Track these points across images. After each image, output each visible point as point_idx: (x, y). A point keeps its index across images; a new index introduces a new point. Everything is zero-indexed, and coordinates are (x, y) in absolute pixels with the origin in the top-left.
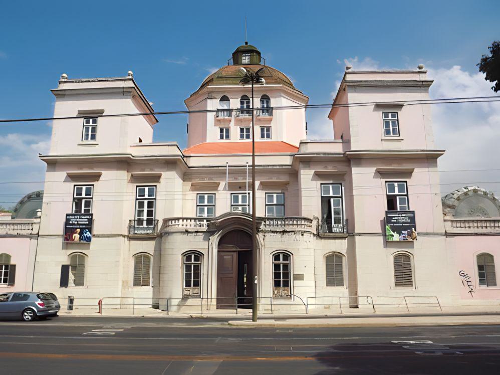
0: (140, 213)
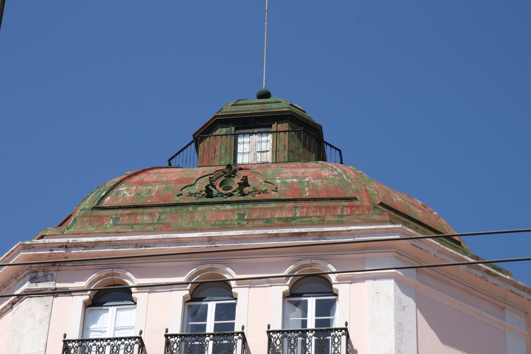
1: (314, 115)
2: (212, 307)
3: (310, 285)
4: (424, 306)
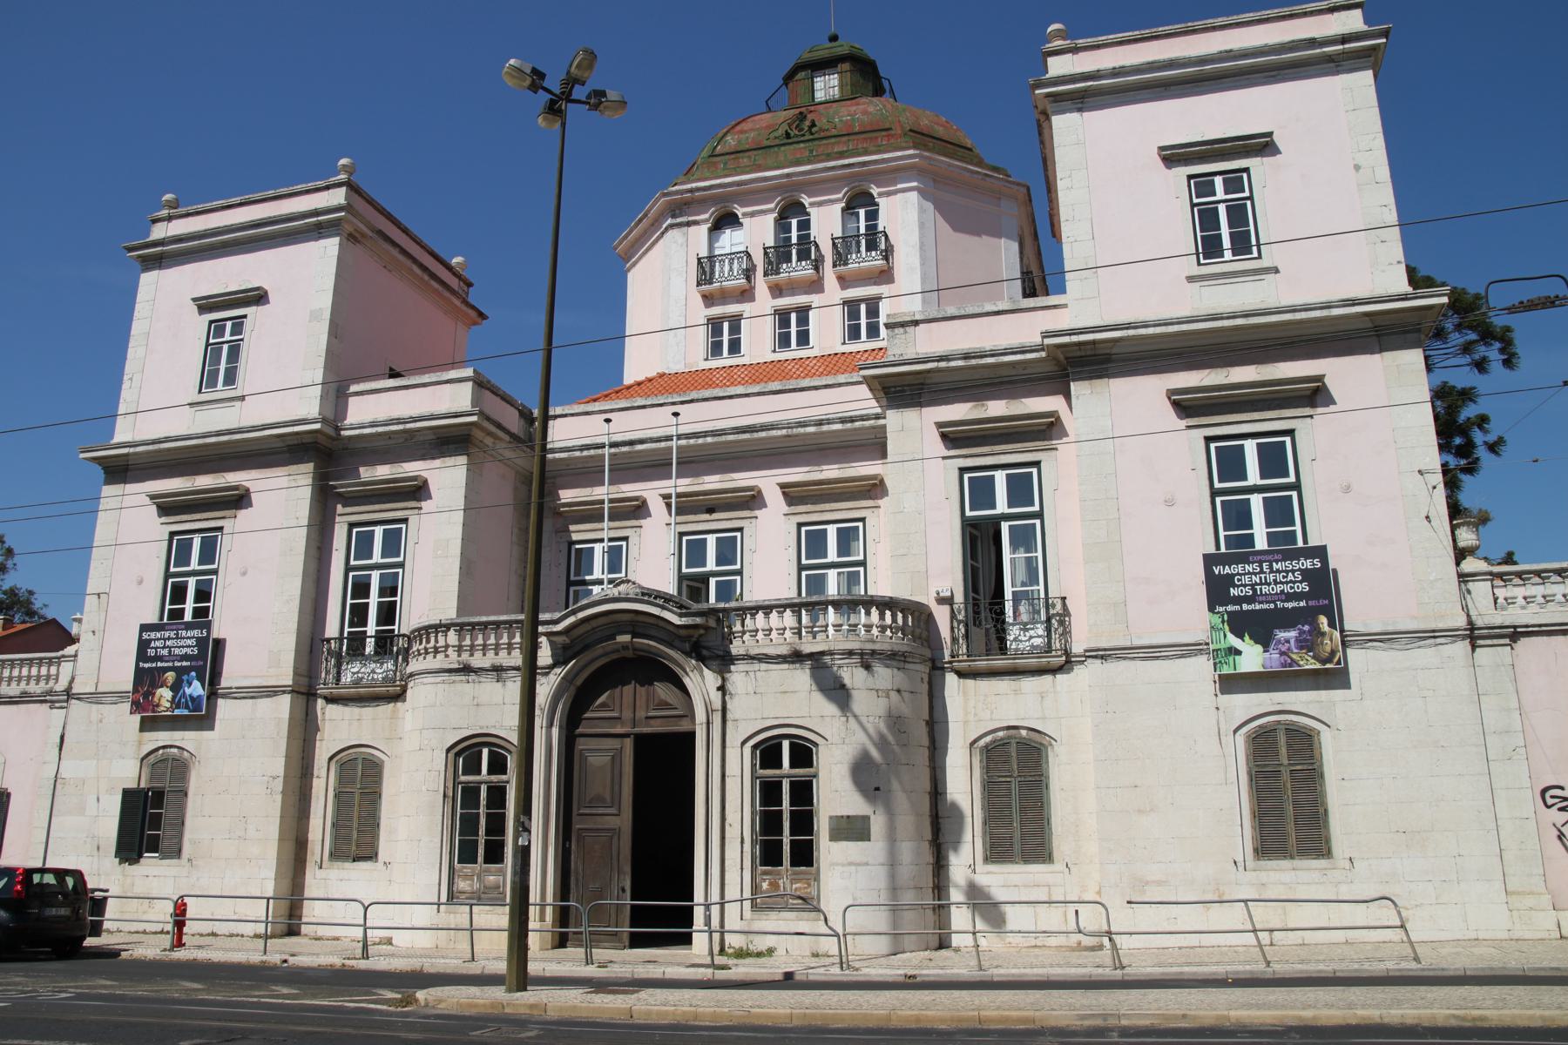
0: (1238, 516)
1: (871, 54)
2: (794, 222)
3: (859, 200)
4: (940, 207)
